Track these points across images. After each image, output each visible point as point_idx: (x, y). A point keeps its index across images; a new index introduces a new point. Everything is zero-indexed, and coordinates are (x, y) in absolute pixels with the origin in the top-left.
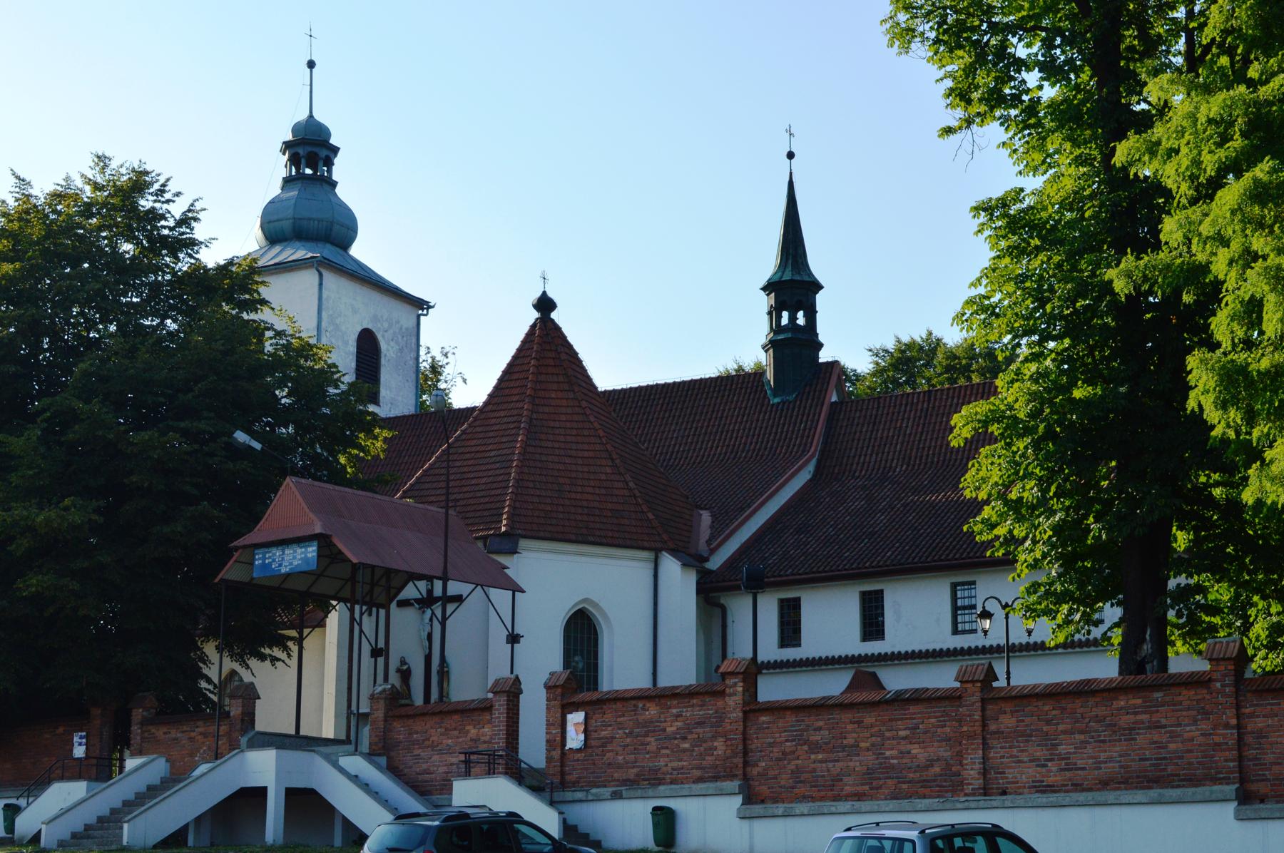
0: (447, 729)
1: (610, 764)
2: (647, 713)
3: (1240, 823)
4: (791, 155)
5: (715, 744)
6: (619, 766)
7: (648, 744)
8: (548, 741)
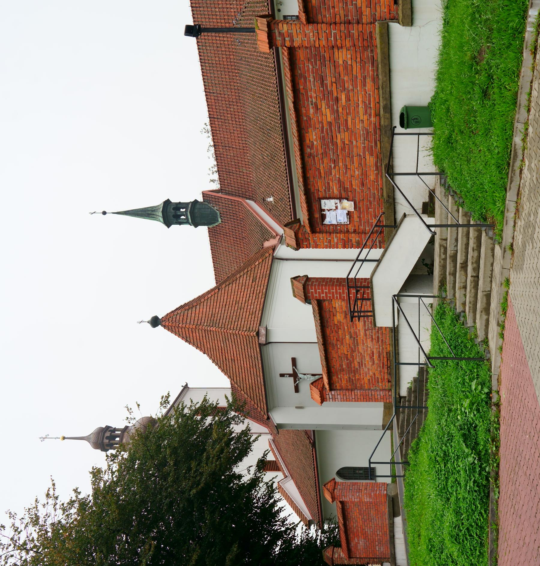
0: (337, 340)
1: (363, 184)
2: (315, 143)
3: (414, 25)
4: (104, 213)
5: (341, 62)
6: (365, 174)
7: (344, 143)
8: (344, 247)
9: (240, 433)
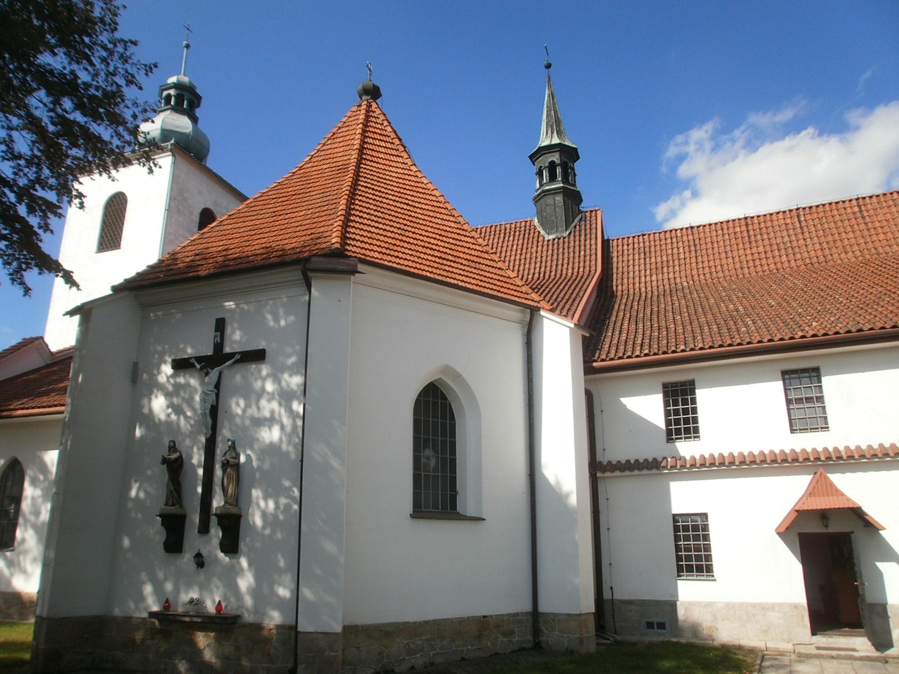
4: (548, 66)
9: (155, 375)
